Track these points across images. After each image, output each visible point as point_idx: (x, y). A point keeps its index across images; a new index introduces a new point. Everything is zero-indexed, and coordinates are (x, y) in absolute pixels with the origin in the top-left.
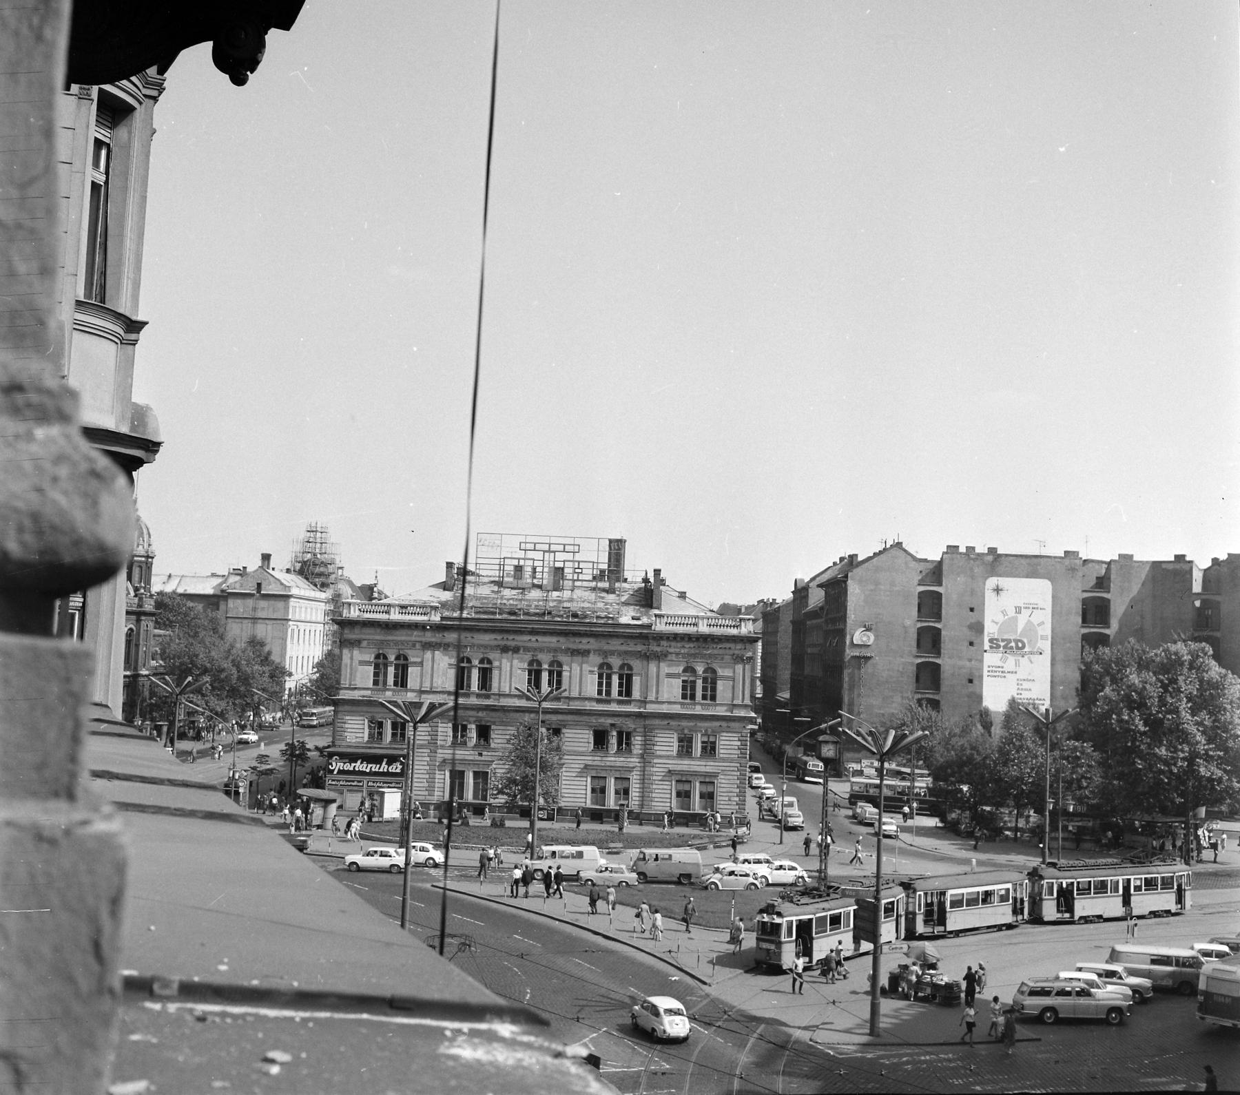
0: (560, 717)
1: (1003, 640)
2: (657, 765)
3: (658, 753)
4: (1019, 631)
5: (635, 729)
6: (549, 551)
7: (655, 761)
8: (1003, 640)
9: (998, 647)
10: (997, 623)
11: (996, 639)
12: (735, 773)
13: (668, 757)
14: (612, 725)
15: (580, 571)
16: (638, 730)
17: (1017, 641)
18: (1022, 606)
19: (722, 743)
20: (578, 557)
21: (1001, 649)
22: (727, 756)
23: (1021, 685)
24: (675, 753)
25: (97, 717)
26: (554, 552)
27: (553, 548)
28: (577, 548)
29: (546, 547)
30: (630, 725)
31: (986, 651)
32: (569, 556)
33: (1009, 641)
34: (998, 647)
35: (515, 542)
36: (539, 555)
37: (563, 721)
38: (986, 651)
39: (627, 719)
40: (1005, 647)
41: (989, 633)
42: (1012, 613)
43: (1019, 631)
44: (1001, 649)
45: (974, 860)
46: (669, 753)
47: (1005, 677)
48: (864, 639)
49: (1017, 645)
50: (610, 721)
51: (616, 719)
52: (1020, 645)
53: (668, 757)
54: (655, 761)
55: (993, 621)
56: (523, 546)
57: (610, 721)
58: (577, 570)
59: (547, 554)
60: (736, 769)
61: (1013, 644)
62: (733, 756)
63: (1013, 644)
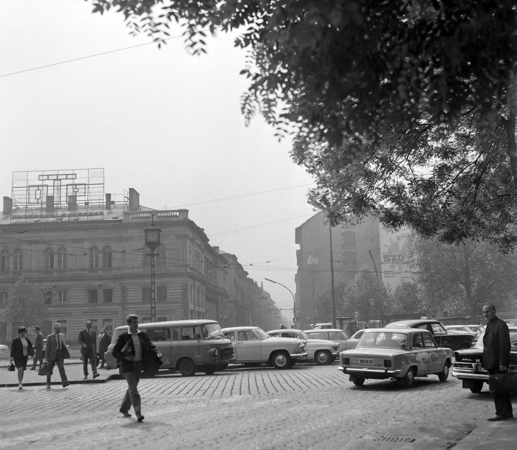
0: (66, 283)
1: (391, 256)
2: (129, 309)
3: (129, 301)
4: (400, 250)
5: (114, 287)
6: (57, 180)
7: (128, 306)
8: (391, 256)
9: (389, 260)
10: (387, 247)
11: (387, 256)
12: (180, 311)
13: (136, 304)
14: (100, 286)
15: (77, 190)
16: (116, 288)
17: (399, 256)
18: (401, 236)
19: (170, 291)
20: (76, 182)
21: (391, 261)
22: (174, 300)
23: (404, 280)
24: (141, 300)
25: (303, 384)
26: (60, 180)
27: (60, 177)
28: (74, 176)
29: (55, 177)
30: (111, 284)
31: (382, 263)
32: (70, 182)
33: (395, 256)
34: (389, 260)
35: (35, 176)
36: (50, 183)
37: (68, 285)
38: (382, 263)
39: (109, 281)
40: (393, 260)
41: (383, 253)
42: (395, 240)
43: (400, 250)
44: (391, 261)
45: (94, 254)
46: (137, 301)
47: (394, 277)
48: (314, 261)
49: (399, 258)
50: (98, 283)
51: (102, 282)
52: (401, 258)
53: (136, 304)
54: (128, 306)
55: (385, 246)
56: (41, 178)
57: (98, 283)
58: (75, 190)
59: (56, 182)
60: (180, 308)
61: (397, 258)
62: (177, 299)
63: (397, 258)
